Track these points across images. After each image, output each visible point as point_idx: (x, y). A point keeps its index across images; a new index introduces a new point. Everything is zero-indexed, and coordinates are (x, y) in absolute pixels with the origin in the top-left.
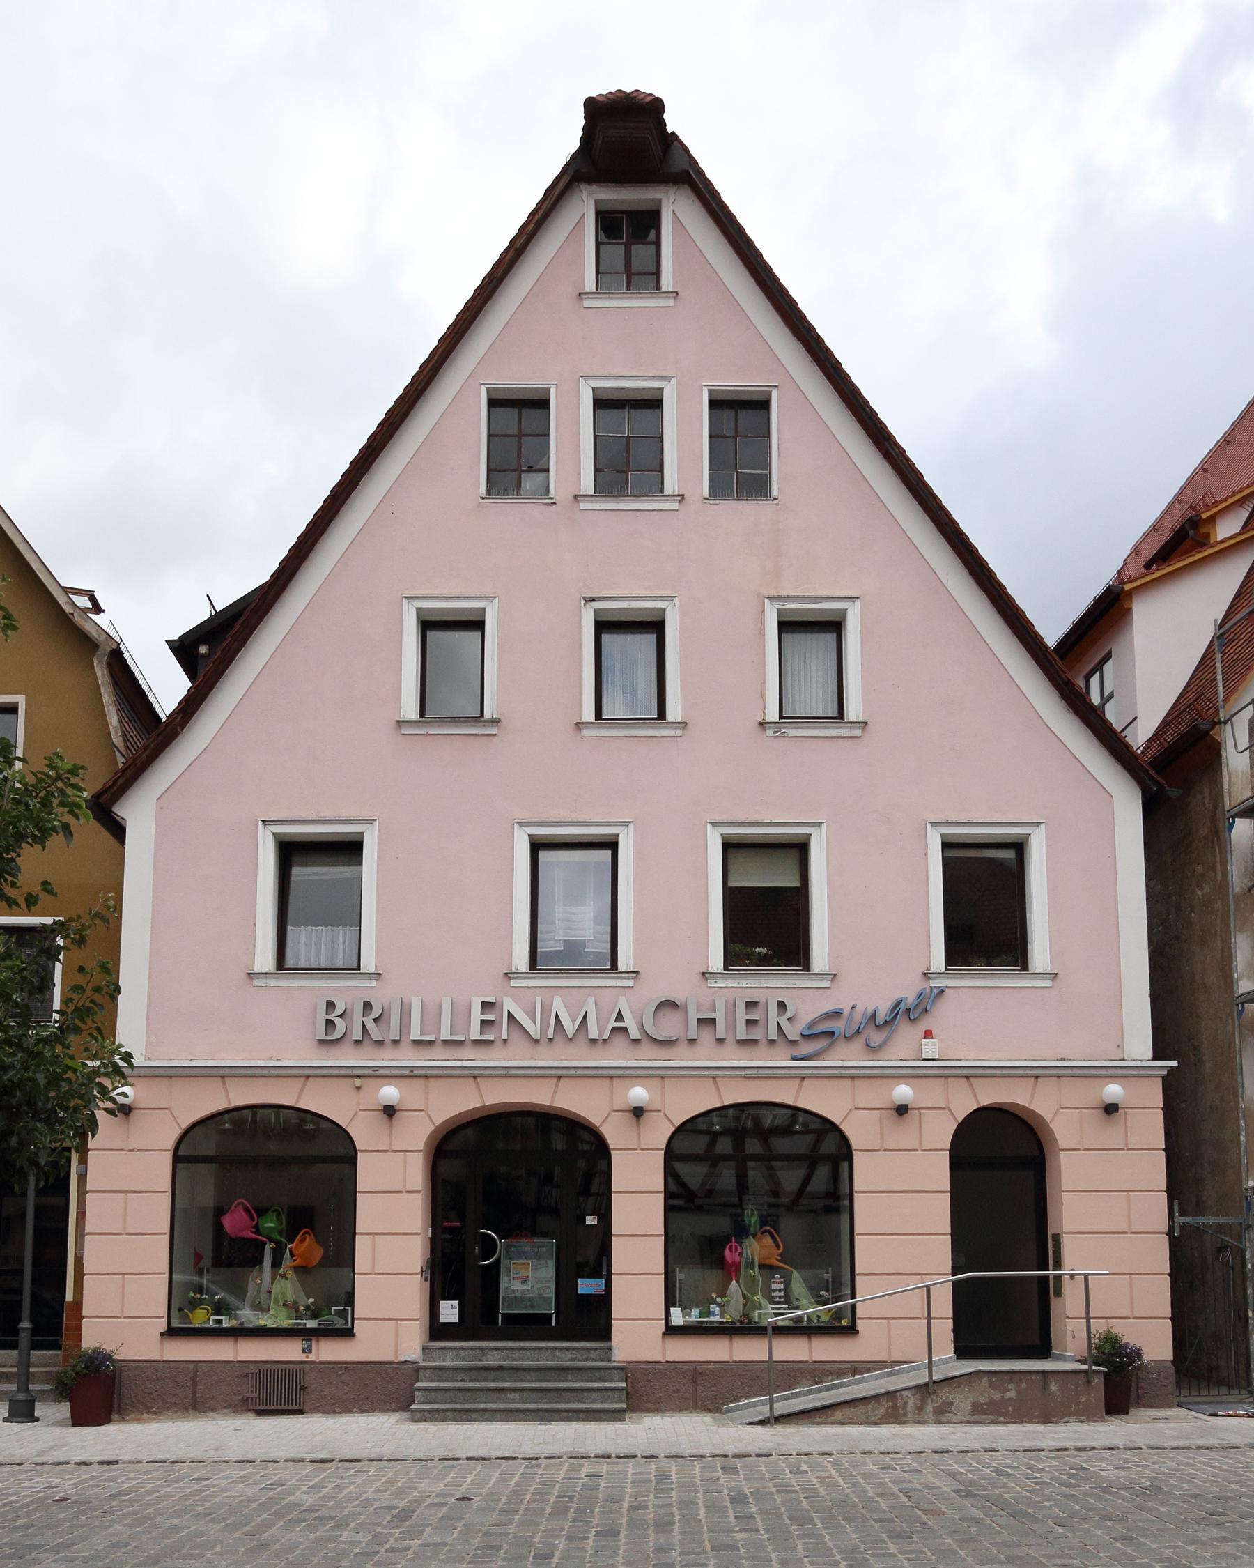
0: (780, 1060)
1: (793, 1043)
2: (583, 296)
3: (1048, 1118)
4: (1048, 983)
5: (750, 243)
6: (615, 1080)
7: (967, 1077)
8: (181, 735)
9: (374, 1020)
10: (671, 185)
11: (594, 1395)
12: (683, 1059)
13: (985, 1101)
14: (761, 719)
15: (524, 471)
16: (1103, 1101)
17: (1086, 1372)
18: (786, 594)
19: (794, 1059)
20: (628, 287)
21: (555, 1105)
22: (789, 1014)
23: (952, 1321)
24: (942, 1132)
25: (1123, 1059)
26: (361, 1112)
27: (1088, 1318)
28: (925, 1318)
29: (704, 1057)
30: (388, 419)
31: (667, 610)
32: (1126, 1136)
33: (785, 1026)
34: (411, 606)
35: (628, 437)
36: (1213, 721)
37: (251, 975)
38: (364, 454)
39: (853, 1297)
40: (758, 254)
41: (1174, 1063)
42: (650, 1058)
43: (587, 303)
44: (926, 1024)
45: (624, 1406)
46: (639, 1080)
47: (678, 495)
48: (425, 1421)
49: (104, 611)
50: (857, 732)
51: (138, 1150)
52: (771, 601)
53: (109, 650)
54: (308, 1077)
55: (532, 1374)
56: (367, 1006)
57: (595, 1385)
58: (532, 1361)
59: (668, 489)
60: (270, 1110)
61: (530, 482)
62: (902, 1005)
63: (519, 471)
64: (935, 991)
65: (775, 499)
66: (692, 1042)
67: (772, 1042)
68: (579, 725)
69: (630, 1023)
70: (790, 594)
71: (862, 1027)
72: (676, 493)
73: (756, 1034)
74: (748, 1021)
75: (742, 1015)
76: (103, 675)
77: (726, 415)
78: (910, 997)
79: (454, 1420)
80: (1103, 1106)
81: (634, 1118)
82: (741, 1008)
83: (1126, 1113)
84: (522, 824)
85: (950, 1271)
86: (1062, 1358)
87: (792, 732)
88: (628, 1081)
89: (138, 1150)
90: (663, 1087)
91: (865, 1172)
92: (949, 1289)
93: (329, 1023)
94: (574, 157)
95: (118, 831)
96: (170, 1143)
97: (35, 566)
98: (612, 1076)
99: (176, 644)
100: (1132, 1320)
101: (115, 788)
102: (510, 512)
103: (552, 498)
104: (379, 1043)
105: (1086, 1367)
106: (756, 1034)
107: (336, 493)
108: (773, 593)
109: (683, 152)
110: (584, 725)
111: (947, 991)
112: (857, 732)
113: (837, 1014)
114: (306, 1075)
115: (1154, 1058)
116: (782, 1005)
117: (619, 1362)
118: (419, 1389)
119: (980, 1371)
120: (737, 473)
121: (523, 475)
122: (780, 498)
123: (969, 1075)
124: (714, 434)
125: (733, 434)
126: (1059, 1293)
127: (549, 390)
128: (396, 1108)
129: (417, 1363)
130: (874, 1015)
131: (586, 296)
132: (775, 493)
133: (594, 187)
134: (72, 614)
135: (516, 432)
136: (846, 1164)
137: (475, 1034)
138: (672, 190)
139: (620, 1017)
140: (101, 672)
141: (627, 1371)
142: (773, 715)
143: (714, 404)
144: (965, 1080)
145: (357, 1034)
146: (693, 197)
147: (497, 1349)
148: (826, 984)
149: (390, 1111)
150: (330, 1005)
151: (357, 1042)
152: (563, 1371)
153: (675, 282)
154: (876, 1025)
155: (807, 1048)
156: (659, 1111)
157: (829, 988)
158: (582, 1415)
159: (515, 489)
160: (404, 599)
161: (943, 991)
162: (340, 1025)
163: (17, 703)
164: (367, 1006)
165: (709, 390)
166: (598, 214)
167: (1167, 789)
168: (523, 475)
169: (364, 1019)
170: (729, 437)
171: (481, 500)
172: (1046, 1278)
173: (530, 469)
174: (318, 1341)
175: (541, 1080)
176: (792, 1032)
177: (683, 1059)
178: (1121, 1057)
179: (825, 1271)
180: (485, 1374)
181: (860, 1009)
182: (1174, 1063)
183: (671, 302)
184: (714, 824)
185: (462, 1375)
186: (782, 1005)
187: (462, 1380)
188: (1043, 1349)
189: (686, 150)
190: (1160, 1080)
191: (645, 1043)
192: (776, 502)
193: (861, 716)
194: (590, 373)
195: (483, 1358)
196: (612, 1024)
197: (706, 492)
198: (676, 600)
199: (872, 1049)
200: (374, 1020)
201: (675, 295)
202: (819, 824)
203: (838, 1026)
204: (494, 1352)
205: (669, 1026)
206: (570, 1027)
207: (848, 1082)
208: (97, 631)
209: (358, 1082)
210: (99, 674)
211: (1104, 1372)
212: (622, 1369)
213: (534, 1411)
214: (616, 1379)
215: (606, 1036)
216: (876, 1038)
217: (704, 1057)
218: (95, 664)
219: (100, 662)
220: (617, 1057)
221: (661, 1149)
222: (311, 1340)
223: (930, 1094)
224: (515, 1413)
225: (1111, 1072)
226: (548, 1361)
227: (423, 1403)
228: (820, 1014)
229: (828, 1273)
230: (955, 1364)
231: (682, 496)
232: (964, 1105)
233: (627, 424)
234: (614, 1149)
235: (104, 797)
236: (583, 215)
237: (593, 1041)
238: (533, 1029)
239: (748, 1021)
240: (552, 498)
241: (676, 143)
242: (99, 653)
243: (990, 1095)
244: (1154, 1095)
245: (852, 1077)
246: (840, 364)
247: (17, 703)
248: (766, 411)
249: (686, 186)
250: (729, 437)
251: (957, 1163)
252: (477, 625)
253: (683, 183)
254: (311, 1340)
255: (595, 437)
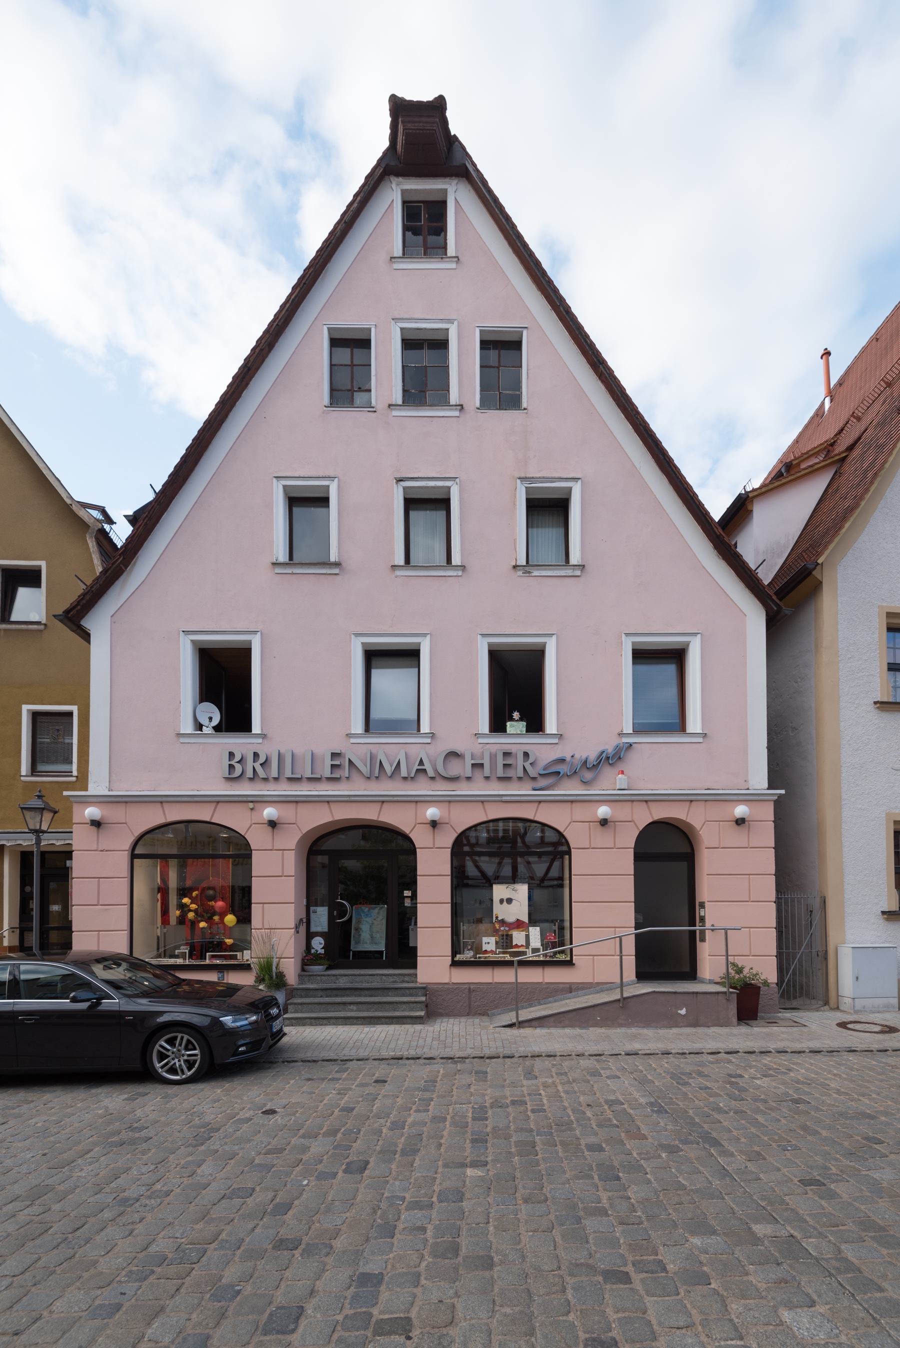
0: (524, 790)
1: (534, 779)
2: (393, 260)
3: (698, 826)
4: (701, 740)
5: (508, 218)
6: (452, 804)
7: (646, 801)
8: (125, 574)
9: (261, 764)
10: (454, 178)
11: (404, 1006)
12: (464, 790)
13: (657, 817)
14: (514, 564)
15: (356, 391)
16: (736, 817)
17: (725, 993)
18: (531, 476)
19: (534, 789)
20: (425, 254)
21: (380, 819)
22: (531, 760)
23: (634, 957)
24: (628, 838)
25: (748, 789)
26: (254, 825)
27: (727, 956)
28: (618, 955)
29: (479, 789)
30: (259, 346)
31: (452, 489)
32: (536, 812)
33: (529, 768)
34: (279, 484)
35: (426, 366)
36: (816, 562)
37: (179, 735)
38: (242, 372)
39: (571, 944)
40: (513, 226)
41: (783, 792)
42: (442, 789)
43: (396, 266)
44: (621, 766)
45: (422, 1013)
46: (432, 804)
47: (459, 405)
48: (292, 1026)
49: (115, 523)
50: (578, 573)
51: (107, 851)
52: (521, 481)
53: (96, 529)
54: (218, 802)
55: (366, 992)
56: (256, 755)
57: (405, 999)
58: (368, 983)
59: (453, 402)
60: (182, 825)
61: (359, 398)
62: (604, 755)
63: (352, 391)
64: (627, 745)
65: (525, 409)
66: (468, 778)
67: (520, 778)
68: (394, 567)
69: (427, 766)
70: (534, 476)
71: (578, 768)
72: (458, 404)
73: (510, 773)
74: (504, 765)
75: (500, 761)
76: (93, 547)
77: (493, 354)
78: (610, 749)
79: (311, 1025)
80: (735, 819)
81: (432, 828)
82: (500, 757)
83: (749, 824)
84: (357, 635)
85: (633, 924)
86: (702, 981)
87: (536, 573)
88: (597, 804)
89: (107, 851)
90: (449, 807)
91: (579, 862)
92: (632, 939)
93: (231, 767)
94: (385, 154)
95: (86, 636)
96: (127, 844)
97: (45, 472)
98: (418, 801)
99: (131, 518)
100: (751, 957)
101: (79, 607)
102: (346, 417)
103: (373, 407)
104: (266, 780)
105: (724, 990)
106: (510, 773)
107: (224, 400)
108: (523, 475)
109: (461, 149)
110: (397, 568)
111: (634, 745)
112: (578, 573)
113: (562, 761)
114: (218, 801)
115: (768, 789)
116: (526, 755)
117: (422, 984)
118: (291, 1004)
119: (654, 992)
120: (500, 393)
121: (355, 394)
122: (529, 408)
123: (647, 800)
124: (484, 365)
125: (497, 365)
126: (703, 940)
127: (370, 330)
128: (277, 822)
129: (293, 985)
130: (586, 762)
131: (396, 260)
132: (524, 405)
133: (400, 179)
134: (71, 505)
135: (349, 363)
136: (567, 857)
137: (327, 773)
138: (454, 181)
139: (421, 762)
140: (92, 544)
141: (425, 989)
142: (522, 561)
143: (485, 344)
144: (644, 803)
145: (250, 774)
146: (469, 187)
147: (345, 975)
148: (556, 741)
149: (273, 824)
150: (231, 755)
151: (250, 779)
152: (385, 990)
153: (457, 250)
154: (588, 768)
155: (543, 782)
156: (448, 823)
157: (557, 744)
158: (394, 1020)
159: (350, 402)
160: (274, 479)
161: (631, 745)
162: (238, 769)
163: (41, 566)
164: (256, 755)
165: (481, 331)
166: (404, 202)
167: (784, 608)
168: (355, 394)
169: (254, 764)
170: (494, 367)
171: (325, 408)
172: (695, 931)
173: (360, 390)
174: (228, 972)
175: (624, 803)
176: (532, 772)
177: (464, 790)
178: (746, 787)
179: (553, 924)
180: (335, 992)
181: (577, 756)
182: (783, 792)
183: (454, 266)
184: (483, 635)
185: (320, 993)
186: (526, 755)
187: (321, 997)
188: (691, 974)
189: (463, 148)
190: (772, 803)
191: (437, 778)
192: (525, 411)
193: (580, 561)
194: (398, 317)
195: (337, 981)
196: (416, 767)
197: (478, 404)
198: (458, 480)
199: (585, 783)
200: (261, 764)
201: (456, 259)
202: (551, 635)
203: (562, 769)
204: (344, 977)
205: (455, 768)
206: (389, 769)
207: (569, 804)
208: (88, 516)
209: (251, 805)
210: (90, 545)
211: (737, 993)
212: (424, 988)
213: (364, 1018)
214: (420, 994)
215: (412, 775)
216: (588, 775)
217: (479, 789)
218: (88, 539)
219: (91, 537)
220: (421, 789)
221: (449, 848)
222: (223, 972)
223: (623, 812)
224: (351, 1020)
225: (741, 798)
226: (378, 982)
227: (294, 1012)
228: (551, 760)
229: (555, 925)
230: (637, 985)
231: (462, 405)
232: (644, 817)
233: (426, 357)
234: (418, 848)
235: (72, 613)
236: (393, 200)
237: (405, 778)
238: (365, 770)
239: (504, 765)
240: (373, 407)
241: (457, 143)
242: (90, 531)
243: (661, 813)
244: (768, 812)
245: (572, 801)
246: (570, 308)
247: (41, 566)
248: (520, 352)
249: (464, 179)
250: (494, 367)
251: (639, 857)
252: (324, 501)
253: (462, 177)
254: (223, 972)
255: (403, 367)
